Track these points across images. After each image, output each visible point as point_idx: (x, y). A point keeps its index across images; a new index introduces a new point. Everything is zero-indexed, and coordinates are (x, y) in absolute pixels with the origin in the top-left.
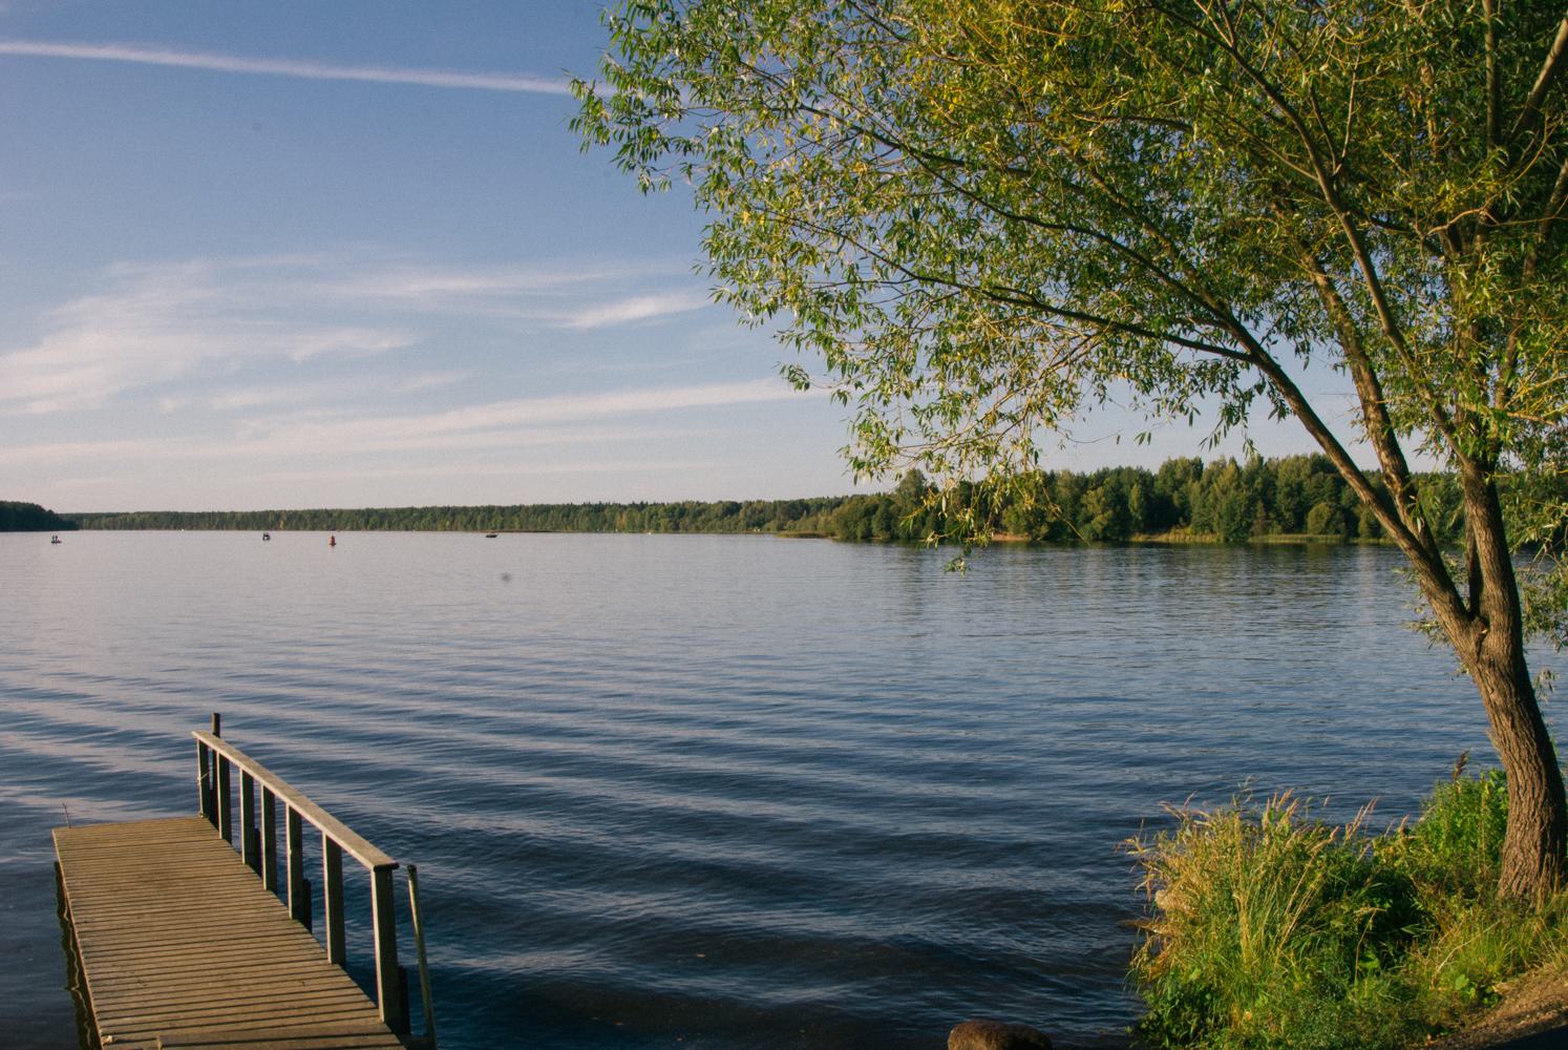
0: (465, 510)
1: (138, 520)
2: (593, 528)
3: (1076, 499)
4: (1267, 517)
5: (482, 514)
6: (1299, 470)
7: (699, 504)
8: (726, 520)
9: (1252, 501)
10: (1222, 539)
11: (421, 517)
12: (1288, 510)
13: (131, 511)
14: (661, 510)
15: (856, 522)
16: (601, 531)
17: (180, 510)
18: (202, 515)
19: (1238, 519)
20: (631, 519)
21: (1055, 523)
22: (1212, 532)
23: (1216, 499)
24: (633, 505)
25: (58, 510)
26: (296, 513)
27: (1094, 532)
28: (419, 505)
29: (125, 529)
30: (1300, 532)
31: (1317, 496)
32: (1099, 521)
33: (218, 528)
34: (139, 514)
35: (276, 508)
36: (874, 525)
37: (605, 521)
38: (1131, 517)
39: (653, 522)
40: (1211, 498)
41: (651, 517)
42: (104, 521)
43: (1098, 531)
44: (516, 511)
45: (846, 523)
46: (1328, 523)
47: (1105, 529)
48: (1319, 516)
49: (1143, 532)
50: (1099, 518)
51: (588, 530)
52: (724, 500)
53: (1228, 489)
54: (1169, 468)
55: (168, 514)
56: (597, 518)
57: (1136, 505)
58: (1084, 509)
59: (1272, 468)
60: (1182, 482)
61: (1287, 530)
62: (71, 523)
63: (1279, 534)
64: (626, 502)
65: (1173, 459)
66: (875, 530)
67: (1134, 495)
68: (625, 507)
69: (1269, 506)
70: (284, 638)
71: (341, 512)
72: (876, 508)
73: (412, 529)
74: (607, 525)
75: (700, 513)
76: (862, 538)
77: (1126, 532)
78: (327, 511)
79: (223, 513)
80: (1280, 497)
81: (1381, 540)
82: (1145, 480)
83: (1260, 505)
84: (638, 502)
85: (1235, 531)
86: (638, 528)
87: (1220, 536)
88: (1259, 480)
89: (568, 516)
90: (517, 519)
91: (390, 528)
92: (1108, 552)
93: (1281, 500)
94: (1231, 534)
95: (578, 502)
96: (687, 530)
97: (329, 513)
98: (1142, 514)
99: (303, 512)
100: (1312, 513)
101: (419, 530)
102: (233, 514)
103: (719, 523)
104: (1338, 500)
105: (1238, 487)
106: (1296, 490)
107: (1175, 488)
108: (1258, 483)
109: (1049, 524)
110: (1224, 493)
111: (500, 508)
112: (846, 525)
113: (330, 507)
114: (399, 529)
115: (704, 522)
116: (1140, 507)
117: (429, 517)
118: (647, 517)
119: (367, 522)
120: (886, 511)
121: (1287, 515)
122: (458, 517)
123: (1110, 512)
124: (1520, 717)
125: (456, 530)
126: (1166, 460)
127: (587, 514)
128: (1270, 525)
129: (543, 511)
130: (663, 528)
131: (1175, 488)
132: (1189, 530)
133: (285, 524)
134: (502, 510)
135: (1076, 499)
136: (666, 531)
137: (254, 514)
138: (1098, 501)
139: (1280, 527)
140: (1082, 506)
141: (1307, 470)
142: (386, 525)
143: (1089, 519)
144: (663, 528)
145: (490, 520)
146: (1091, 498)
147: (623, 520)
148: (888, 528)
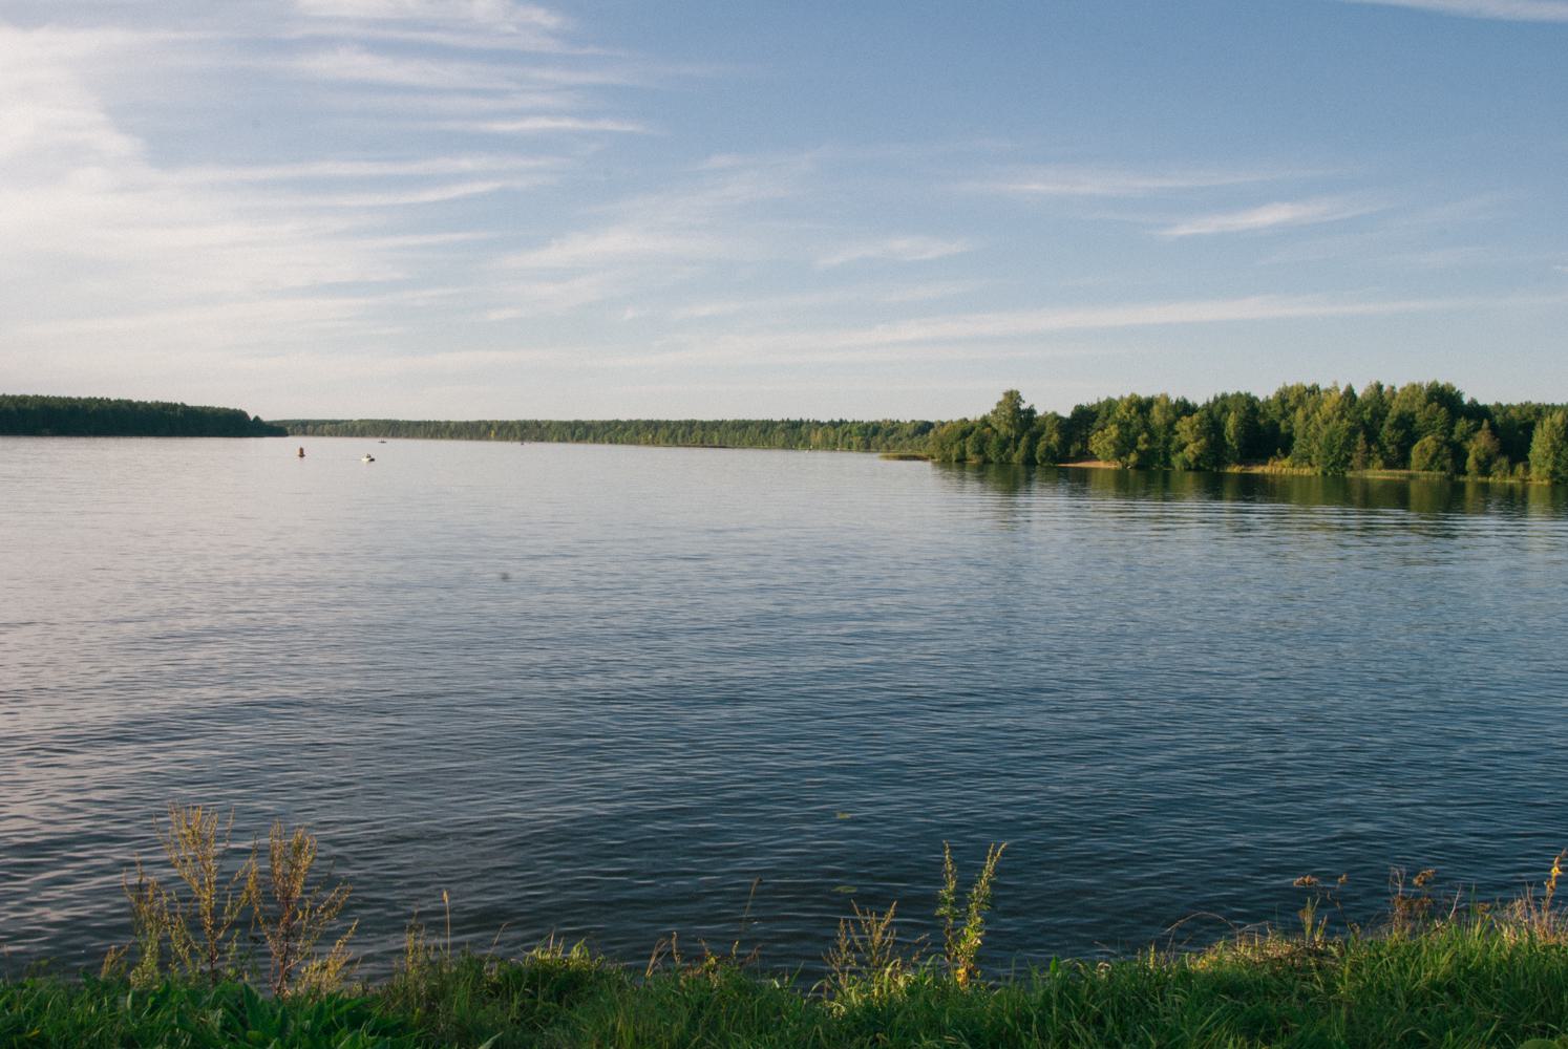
0: (668, 423)
1: (358, 428)
2: (789, 445)
3: (1170, 426)
4: (1369, 450)
5: (683, 428)
6: (1413, 400)
9: (1353, 432)
10: (1319, 473)
11: (625, 430)
12: (1391, 443)
13: (355, 418)
15: (952, 444)
17: (400, 418)
19: (1336, 451)
20: (825, 436)
21: (1146, 450)
22: (1311, 465)
23: (1318, 429)
24: (833, 424)
25: (266, 418)
26: (507, 423)
27: (1185, 462)
28: (624, 418)
29: (346, 436)
30: (1404, 468)
31: (1429, 427)
32: (1192, 450)
33: (432, 437)
34: (361, 421)
35: (488, 418)
36: (968, 448)
37: (800, 439)
38: (1226, 446)
39: (846, 439)
40: (1312, 427)
41: (845, 435)
42: (327, 427)
43: (1190, 461)
45: (943, 444)
46: (1433, 459)
47: (1197, 459)
48: (1423, 450)
49: (1239, 463)
50: (1191, 447)
51: (784, 447)
52: (917, 419)
53: (1331, 419)
54: (1283, 397)
55: (386, 422)
56: (793, 434)
57: (1232, 434)
58: (1176, 437)
61: (1389, 465)
62: (277, 430)
63: (1380, 469)
64: (825, 419)
65: (1289, 385)
66: (969, 454)
67: (1231, 422)
68: (823, 424)
69: (1372, 436)
70: (1519, 853)
71: (550, 423)
73: (616, 442)
74: (802, 441)
75: (892, 432)
76: (957, 461)
77: (1220, 462)
78: (536, 422)
79: (439, 422)
80: (1385, 428)
81: (1491, 479)
83: (1361, 436)
84: (837, 420)
85: (1332, 465)
86: (831, 446)
89: (765, 431)
90: (716, 433)
91: (595, 441)
92: (938, 472)
93: (1386, 433)
94: (1328, 468)
95: (777, 418)
96: (878, 450)
97: (538, 424)
98: (1239, 444)
99: (513, 422)
100: (1416, 448)
101: (623, 443)
102: (448, 423)
103: (909, 443)
105: (1341, 418)
106: (1405, 422)
107: (1284, 415)
109: (1139, 451)
111: (702, 422)
112: (942, 447)
113: (540, 418)
114: (603, 442)
115: (895, 441)
118: (840, 435)
119: (573, 434)
121: (1390, 449)
122: (661, 430)
123: (1203, 441)
126: (1282, 386)
128: (1370, 458)
129: (742, 426)
130: (855, 446)
132: (1286, 462)
133: (496, 434)
134: (704, 425)
135: (1170, 426)
136: (858, 450)
138: (1192, 428)
139: (1381, 462)
140: (1177, 433)
142: (591, 438)
143: (1182, 447)
144: (855, 446)
145: (690, 434)
146: (1184, 425)
147: (817, 437)
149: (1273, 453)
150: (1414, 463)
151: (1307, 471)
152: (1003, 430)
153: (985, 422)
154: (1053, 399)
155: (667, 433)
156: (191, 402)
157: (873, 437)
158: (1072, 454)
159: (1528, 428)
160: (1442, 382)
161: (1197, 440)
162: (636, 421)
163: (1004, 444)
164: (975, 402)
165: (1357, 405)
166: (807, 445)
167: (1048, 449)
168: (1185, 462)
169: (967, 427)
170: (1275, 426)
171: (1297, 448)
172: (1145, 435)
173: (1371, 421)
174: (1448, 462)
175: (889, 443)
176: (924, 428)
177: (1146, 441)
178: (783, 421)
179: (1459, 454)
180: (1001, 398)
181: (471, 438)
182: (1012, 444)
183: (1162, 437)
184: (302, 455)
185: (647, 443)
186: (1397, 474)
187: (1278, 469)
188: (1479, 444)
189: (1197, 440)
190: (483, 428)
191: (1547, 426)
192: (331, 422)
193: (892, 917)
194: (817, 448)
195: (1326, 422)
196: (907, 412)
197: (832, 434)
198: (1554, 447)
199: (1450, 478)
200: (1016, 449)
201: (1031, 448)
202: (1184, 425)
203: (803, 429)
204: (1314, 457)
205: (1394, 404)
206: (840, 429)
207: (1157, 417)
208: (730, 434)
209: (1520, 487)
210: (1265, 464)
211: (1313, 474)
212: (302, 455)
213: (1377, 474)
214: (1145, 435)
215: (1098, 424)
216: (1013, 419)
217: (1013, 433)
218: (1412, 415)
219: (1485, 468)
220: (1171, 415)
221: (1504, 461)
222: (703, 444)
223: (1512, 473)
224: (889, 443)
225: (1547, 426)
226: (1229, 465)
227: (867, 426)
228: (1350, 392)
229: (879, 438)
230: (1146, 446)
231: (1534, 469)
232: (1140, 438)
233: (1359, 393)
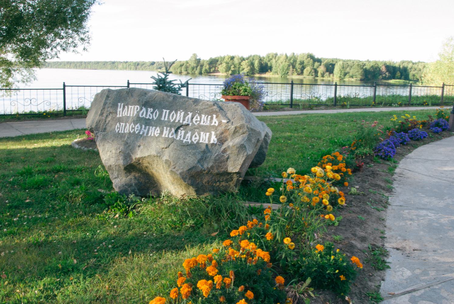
0: (74, 62)
3: (240, 64)
4: (293, 71)
7: (143, 62)
8: (151, 67)
9: (289, 66)
14: (132, 64)
16: (114, 69)
19: (285, 70)
20: (123, 66)
23: (279, 65)
24: (124, 62)
31: (308, 65)
36: (183, 69)
38: (255, 69)
39: (129, 67)
40: (278, 64)
44: (89, 63)
46: (310, 73)
47: (247, 73)
48: (307, 71)
51: (110, 69)
59: (296, 56)
60: (271, 59)
61: (298, 74)
66: (183, 71)
69: (294, 67)
72: (183, 64)
75: (143, 64)
77: (253, 73)
80: (297, 65)
82: (261, 60)
83: (291, 67)
84: (125, 61)
87: (280, 75)
88: (292, 59)
89: (104, 64)
93: (298, 66)
95: (108, 61)
96: (139, 69)
100: (305, 70)
103: (148, 68)
104: (314, 66)
105: (286, 61)
106: (302, 63)
107: (269, 61)
108: (292, 61)
110: (282, 63)
116: (258, 66)
117: (63, 64)
120: (186, 65)
122: (72, 64)
124: (441, 257)
125: (71, 68)
127: (110, 64)
131: (269, 61)
132: (271, 73)
134: (85, 63)
135: (240, 64)
136: (133, 70)
139: (296, 74)
141: (306, 57)
143: (243, 69)
146: (244, 64)
147: (120, 66)
148: (186, 70)
149: (268, 71)
151: (276, 76)
153: (187, 62)
154: (205, 57)
155: (74, 65)
158: (211, 71)
159: (333, 65)
160: (310, 53)
161: (247, 67)
163: (193, 69)
165: (288, 58)
166: (117, 68)
167: (206, 70)
169: (182, 63)
170: (267, 64)
171: (274, 69)
172: (233, 66)
173: (293, 63)
174: (314, 74)
176: (153, 64)
179: (316, 72)
182: (195, 68)
183: (238, 66)
186: (300, 77)
188: (321, 69)
189: (247, 67)
191: (338, 65)
193: (270, 203)
194: (121, 69)
196: (148, 59)
198: (340, 70)
199: (314, 78)
200: (196, 69)
201: (201, 69)
203: (116, 64)
205: (298, 58)
206: (127, 64)
207: (236, 61)
209: (331, 80)
213: (295, 77)
215: (219, 63)
216: (195, 61)
217: (195, 65)
218: (303, 61)
219: (323, 76)
220: (240, 61)
221: (327, 73)
222: (85, 68)
225: (338, 65)
227: (135, 63)
228: (276, 55)
231: (335, 76)
233: (288, 55)
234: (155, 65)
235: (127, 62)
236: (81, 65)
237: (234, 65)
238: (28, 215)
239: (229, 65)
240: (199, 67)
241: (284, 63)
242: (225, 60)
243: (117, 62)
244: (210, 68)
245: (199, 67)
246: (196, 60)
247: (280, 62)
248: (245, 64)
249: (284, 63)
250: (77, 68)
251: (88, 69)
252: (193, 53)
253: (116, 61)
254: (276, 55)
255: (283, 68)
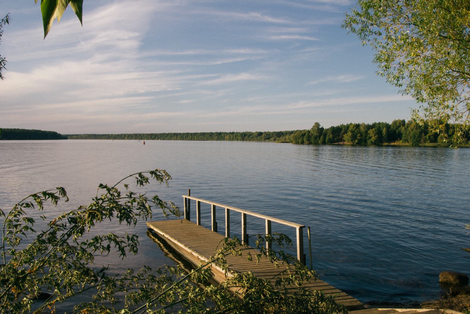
0: (180, 134)
3: (366, 132)
5: (185, 135)
7: (250, 132)
10: (411, 144)
11: (167, 136)
18: (103, 135)
19: (416, 138)
21: (360, 139)
22: (408, 142)
23: (409, 132)
24: (230, 133)
27: (372, 142)
28: (167, 132)
30: (435, 143)
35: (125, 133)
37: (222, 138)
39: (236, 138)
40: (408, 132)
41: (236, 136)
45: (296, 138)
49: (387, 142)
50: (373, 138)
54: (395, 123)
56: (220, 136)
58: (368, 135)
61: (431, 142)
64: (228, 132)
65: (396, 120)
66: (305, 141)
72: (305, 134)
73: (165, 139)
75: (250, 135)
78: (139, 134)
79: (109, 135)
82: (387, 126)
83: (423, 134)
84: (232, 132)
86: (231, 139)
95: (214, 132)
96: (246, 140)
97: (140, 135)
110: (412, 130)
111: (191, 133)
112: (296, 139)
118: (235, 136)
119: (151, 138)
122: (178, 136)
123: (377, 136)
125: (178, 140)
126: (394, 120)
129: (93, 135)
132: (401, 141)
133: (127, 138)
134: (191, 134)
135: (366, 132)
136: (240, 140)
137: (118, 135)
138: (373, 132)
139: (429, 141)
142: (157, 138)
143: (370, 138)
146: (371, 132)
150: (439, 141)
152: (315, 134)
156: (43, 130)
157: (278, 136)
161: (375, 136)
162: (171, 133)
163: (316, 138)
164: (308, 126)
166: (224, 139)
167: (330, 139)
168: (372, 142)
172: (359, 135)
175: (250, 138)
177: (359, 136)
178: (216, 133)
180: (314, 124)
181: (119, 139)
183: (364, 135)
184: (144, 144)
185: (174, 140)
187: (399, 144)
189: (375, 136)
190: (123, 136)
192: (76, 135)
194: (227, 140)
195: (412, 130)
197: (232, 136)
200: (320, 139)
202: (371, 132)
204: (409, 140)
206: (234, 134)
208: (200, 136)
210: (395, 142)
211: (409, 145)
212: (144, 144)
214: (359, 135)
215: (343, 132)
223: (467, 143)
224: (250, 138)
226: (384, 142)
228: (404, 121)
229: (247, 137)
230: (360, 138)
232: (358, 135)
234: (263, 135)
235: (233, 133)
236: (188, 136)
237: (361, 134)
238: (256, 286)
239: (355, 134)
240: (322, 137)
241: (415, 130)
242: (350, 129)
243: (223, 133)
244: (333, 137)
245: (322, 137)
246: (319, 129)
247: (410, 130)
248: (372, 132)
249: (415, 130)
250: (183, 140)
251: (194, 140)
252: (316, 122)
253: (222, 132)
254: (404, 121)
255: (415, 136)
